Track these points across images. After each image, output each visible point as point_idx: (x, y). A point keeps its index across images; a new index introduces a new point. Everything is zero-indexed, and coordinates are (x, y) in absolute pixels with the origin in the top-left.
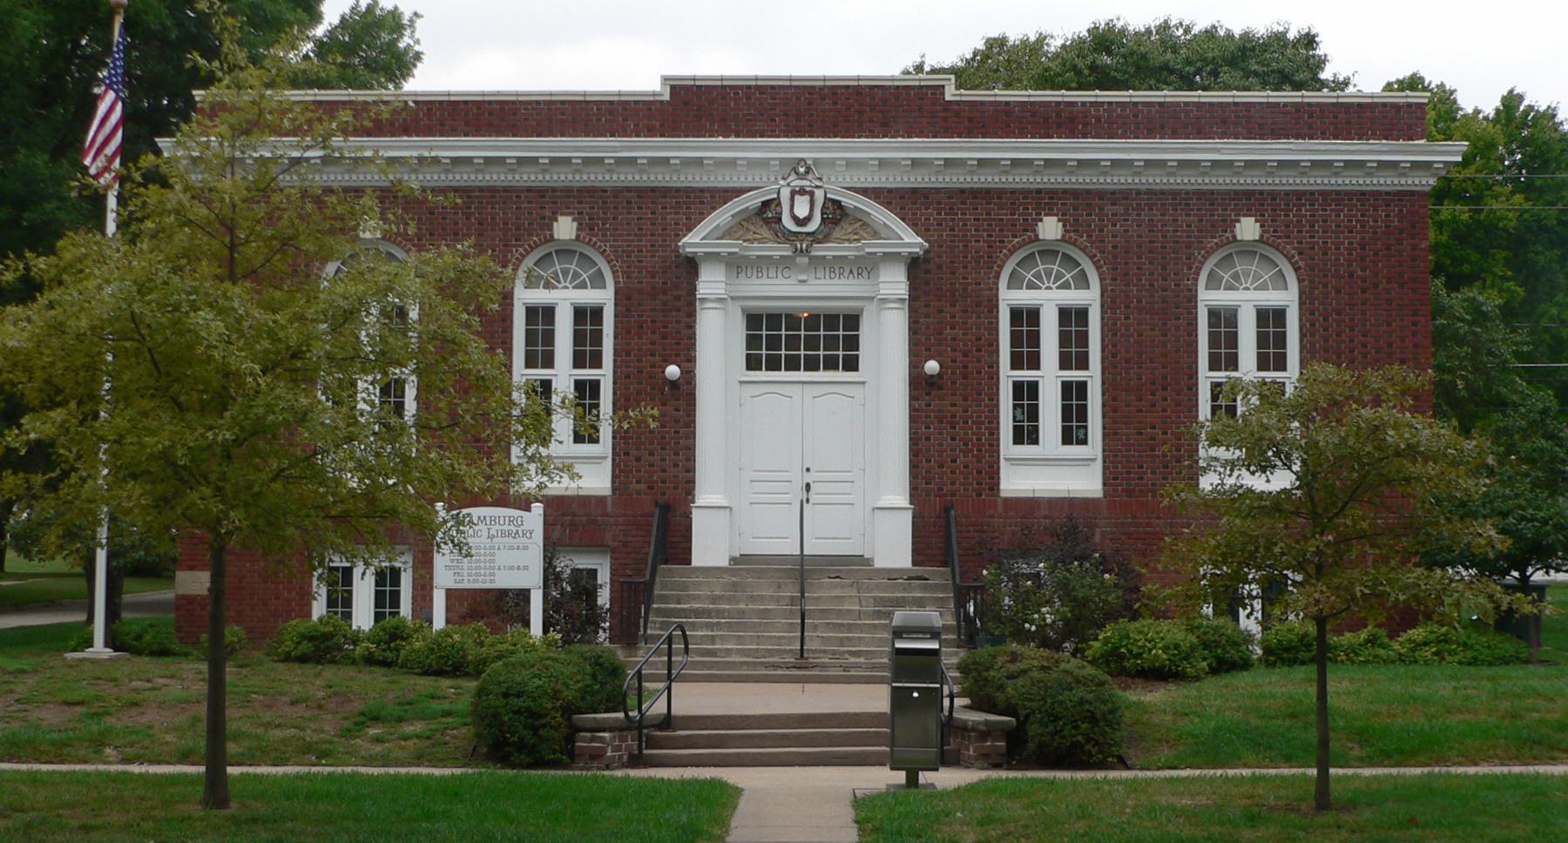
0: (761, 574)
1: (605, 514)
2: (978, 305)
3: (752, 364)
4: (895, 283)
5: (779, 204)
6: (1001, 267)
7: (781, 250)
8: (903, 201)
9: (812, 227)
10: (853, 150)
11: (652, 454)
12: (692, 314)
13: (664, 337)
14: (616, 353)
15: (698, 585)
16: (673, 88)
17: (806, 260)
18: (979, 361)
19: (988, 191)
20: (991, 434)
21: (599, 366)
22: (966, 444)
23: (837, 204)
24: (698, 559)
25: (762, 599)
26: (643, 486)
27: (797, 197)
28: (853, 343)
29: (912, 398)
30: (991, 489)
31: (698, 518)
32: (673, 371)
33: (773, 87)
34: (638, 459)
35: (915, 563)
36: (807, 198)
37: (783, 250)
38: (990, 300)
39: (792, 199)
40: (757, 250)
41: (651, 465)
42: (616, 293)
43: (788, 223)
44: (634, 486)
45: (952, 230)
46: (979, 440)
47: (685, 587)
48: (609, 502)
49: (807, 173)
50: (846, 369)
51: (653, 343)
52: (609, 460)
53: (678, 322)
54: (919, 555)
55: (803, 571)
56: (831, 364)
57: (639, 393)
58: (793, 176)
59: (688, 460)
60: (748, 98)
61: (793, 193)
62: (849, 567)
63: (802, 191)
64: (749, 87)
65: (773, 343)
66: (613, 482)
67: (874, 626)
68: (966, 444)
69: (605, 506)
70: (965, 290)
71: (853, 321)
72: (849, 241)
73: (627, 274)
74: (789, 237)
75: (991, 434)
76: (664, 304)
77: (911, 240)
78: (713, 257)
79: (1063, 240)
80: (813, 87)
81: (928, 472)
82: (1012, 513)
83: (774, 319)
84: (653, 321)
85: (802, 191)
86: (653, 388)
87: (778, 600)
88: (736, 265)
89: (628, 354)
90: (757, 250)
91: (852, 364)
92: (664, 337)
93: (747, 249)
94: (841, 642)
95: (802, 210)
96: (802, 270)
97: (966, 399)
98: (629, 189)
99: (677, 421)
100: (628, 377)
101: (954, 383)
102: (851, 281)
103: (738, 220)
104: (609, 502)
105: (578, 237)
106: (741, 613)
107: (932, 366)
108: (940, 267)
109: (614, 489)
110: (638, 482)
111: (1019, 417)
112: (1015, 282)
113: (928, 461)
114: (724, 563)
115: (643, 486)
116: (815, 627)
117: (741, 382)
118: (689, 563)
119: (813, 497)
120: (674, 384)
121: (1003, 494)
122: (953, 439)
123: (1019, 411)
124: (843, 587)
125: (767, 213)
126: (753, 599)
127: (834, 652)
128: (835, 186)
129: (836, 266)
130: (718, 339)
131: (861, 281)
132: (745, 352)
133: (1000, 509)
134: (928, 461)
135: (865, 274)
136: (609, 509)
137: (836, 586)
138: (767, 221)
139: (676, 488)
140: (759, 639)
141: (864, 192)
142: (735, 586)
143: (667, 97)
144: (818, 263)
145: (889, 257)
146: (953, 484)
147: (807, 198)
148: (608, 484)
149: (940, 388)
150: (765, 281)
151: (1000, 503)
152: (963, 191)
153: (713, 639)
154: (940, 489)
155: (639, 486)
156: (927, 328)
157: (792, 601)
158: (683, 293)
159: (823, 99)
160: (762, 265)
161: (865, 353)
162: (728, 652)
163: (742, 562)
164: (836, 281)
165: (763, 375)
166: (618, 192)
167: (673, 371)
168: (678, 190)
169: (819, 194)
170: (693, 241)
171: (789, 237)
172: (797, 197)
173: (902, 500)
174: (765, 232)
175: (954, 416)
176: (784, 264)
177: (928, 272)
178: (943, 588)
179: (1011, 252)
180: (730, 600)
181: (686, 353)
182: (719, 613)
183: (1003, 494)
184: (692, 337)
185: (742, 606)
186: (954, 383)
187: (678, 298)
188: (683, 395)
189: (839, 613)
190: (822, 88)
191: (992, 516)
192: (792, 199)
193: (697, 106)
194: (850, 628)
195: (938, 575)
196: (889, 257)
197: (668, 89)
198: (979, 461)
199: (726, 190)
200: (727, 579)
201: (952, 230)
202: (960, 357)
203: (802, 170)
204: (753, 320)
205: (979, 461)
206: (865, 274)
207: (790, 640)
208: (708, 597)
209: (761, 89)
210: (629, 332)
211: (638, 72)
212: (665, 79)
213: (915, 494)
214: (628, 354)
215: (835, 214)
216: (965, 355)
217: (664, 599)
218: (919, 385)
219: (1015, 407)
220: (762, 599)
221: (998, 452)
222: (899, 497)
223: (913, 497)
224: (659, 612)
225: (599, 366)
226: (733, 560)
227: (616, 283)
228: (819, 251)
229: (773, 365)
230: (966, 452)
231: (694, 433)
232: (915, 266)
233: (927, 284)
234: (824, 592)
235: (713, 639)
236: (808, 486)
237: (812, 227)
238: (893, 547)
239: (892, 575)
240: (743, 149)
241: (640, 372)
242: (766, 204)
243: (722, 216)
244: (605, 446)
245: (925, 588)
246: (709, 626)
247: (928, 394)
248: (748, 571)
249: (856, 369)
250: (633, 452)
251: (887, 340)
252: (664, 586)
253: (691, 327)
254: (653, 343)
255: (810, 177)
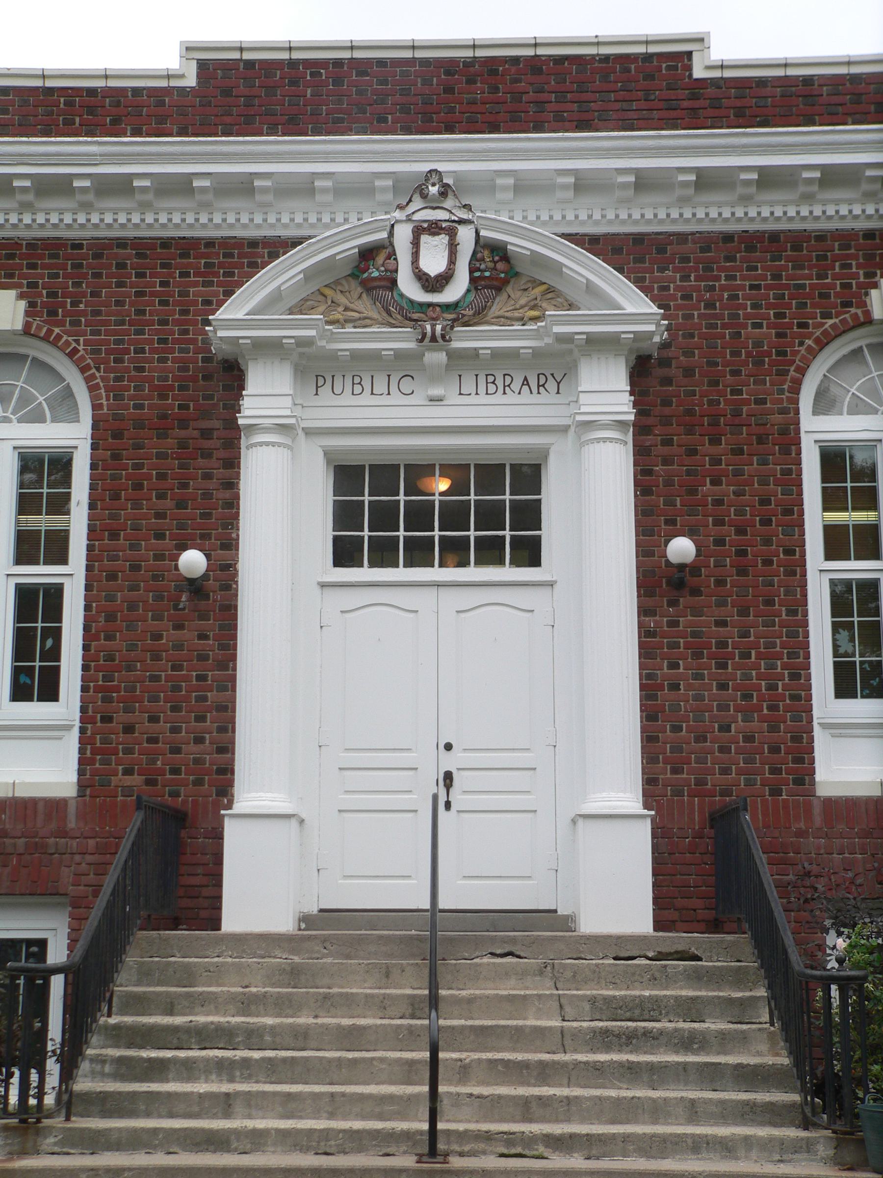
0: (351, 947)
1: (63, 833)
2: (761, 440)
3: (345, 554)
4: (606, 391)
5: (392, 255)
6: (802, 371)
7: (400, 340)
8: (625, 252)
9: (455, 291)
10: (526, 155)
11: (154, 719)
12: (233, 463)
13: (181, 504)
14: (93, 533)
15: (216, 974)
16: (203, 65)
17: (441, 357)
18: (767, 542)
19: (774, 237)
20: (795, 677)
21: (63, 559)
22: (747, 697)
23: (499, 251)
24: (233, 921)
25: (348, 1002)
26: (136, 780)
27: (425, 239)
28: (529, 515)
29: (644, 611)
30: (800, 782)
31: (237, 840)
32: (193, 561)
33: (381, 62)
34: (129, 729)
35: (658, 925)
36: (444, 239)
37: (402, 340)
38: (784, 432)
39: (416, 244)
40: (351, 341)
41: (153, 740)
42: (95, 427)
43: (408, 287)
44: (120, 779)
45: (710, 305)
46: (772, 687)
47: (188, 976)
48: (72, 809)
49: (443, 194)
50: (516, 562)
51: (160, 515)
52: (75, 733)
53: (207, 477)
54: (668, 908)
55: (435, 943)
56: (490, 552)
57: (132, 607)
58: (417, 203)
59: (223, 730)
60: (338, 81)
61: (418, 232)
62: (529, 934)
63: (434, 228)
64: (338, 63)
65: (384, 517)
66: (81, 773)
67: (598, 1068)
68: (747, 697)
69: (64, 818)
70: (737, 414)
71: (529, 476)
72: (522, 320)
73: (117, 393)
74: (411, 314)
75: (795, 677)
76: (183, 445)
77: (633, 308)
78: (269, 349)
79: (27, 330)
80: (453, 61)
81: (677, 749)
82: (841, 827)
83: (384, 475)
84: (162, 477)
85: (434, 228)
86: (159, 598)
87: (383, 1005)
88: (315, 369)
89: (114, 536)
90: (351, 341)
91: (529, 553)
92: (181, 504)
93: (332, 338)
94: (526, 1109)
95: (434, 262)
96: (434, 378)
97: (744, 612)
98: (121, 243)
99: (203, 658)
100: (112, 577)
101: (720, 583)
102: (526, 397)
103: (314, 286)
104: (72, 809)
105: (27, 326)
106: (301, 1037)
107: (681, 548)
108: (688, 372)
109: (82, 785)
110: (128, 772)
111: (845, 647)
112: (825, 403)
113: (677, 729)
114: (285, 924)
115: (136, 780)
116: (464, 1072)
117: (323, 585)
118: (215, 924)
119: (456, 796)
120: (195, 587)
121: (822, 791)
122: (723, 687)
123: (844, 634)
124: (523, 974)
125: (369, 270)
126: (327, 1003)
127: (509, 1138)
128: (530, 231)
129: (496, 369)
130: (281, 504)
131: (544, 398)
132: (330, 534)
133: (818, 820)
134: (677, 729)
135: (551, 385)
136: (72, 823)
137: (505, 974)
138: (368, 286)
139: (199, 782)
140: (334, 1105)
141: (593, 244)
142: (294, 974)
143: (191, 81)
144: (463, 362)
145: (597, 344)
146: (725, 771)
147: (444, 239)
148: (72, 777)
149: (696, 592)
150: (366, 399)
151: (817, 810)
152: (728, 238)
153: (225, 1104)
154: (700, 782)
155: (129, 780)
156: (669, 483)
157: (414, 1008)
158: (216, 424)
159: (471, 81)
160: (361, 368)
161: (553, 532)
162: (257, 1140)
163: (330, 928)
164: (499, 398)
165: (365, 573)
166: (102, 248)
167: (193, 561)
168: (210, 243)
169: (466, 235)
170: (237, 315)
171: (411, 314)
172: (425, 239)
173: (630, 800)
174: (365, 306)
175: (723, 644)
176: (403, 367)
177: (667, 381)
178: (738, 978)
179: (822, 344)
180: (281, 1005)
181: (219, 529)
182: (253, 1037)
183: (822, 791)
184: (233, 504)
185: (304, 1020)
186: (720, 583)
187: (206, 434)
188: (214, 604)
189: (519, 1037)
190: (470, 63)
191: (800, 834)
192: (416, 244)
193: (249, 92)
194: (544, 1073)
195: (728, 952)
196: (597, 344)
197: (194, 65)
198: (774, 729)
199: (253, 243)
200: (280, 959)
201: (710, 305)
202: (732, 536)
203: (434, 190)
204: (346, 476)
205: (774, 729)
206: (551, 385)
207: (401, 1106)
208: (233, 998)
209: (361, 67)
210: (116, 497)
211: (147, 46)
212: (189, 48)
213: (658, 786)
214: (114, 536)
215: (496, 270)
216: (741, 531)
217: (138, 1004)
218: (659, 587)
219: (836, 627)
220: (348, 1002)
221: (809, 710)
222: (620, 790)
223: (650, 798)
224: (119, 1036)
225: (63, 559)
226: (306, 920)
227: (96, 407)
228: (465, 340)
229: (383, 555)
230: (748, 712)
231: (233, 679)
232: (643, 370)
233: (666, 403)
234: (481, 987)
235: (225, 1104)
236: (448, 778)
237: (455, 291)
238: (614, 889)
239: (621, 949)
240: (327, 157)
241: (135, 568)
242: (367, 254)
243: (280, 276)
244: (68, 705)
245: (698, 978)
246: (225, 1069)
247: (673, 603)
248: (324, 940)
249: (535, 561)
250: (120, 717)
251: (594, 503)
252: (145, 974)
253: (231, 485)
254: (160, 515)
255: (449, 203)
